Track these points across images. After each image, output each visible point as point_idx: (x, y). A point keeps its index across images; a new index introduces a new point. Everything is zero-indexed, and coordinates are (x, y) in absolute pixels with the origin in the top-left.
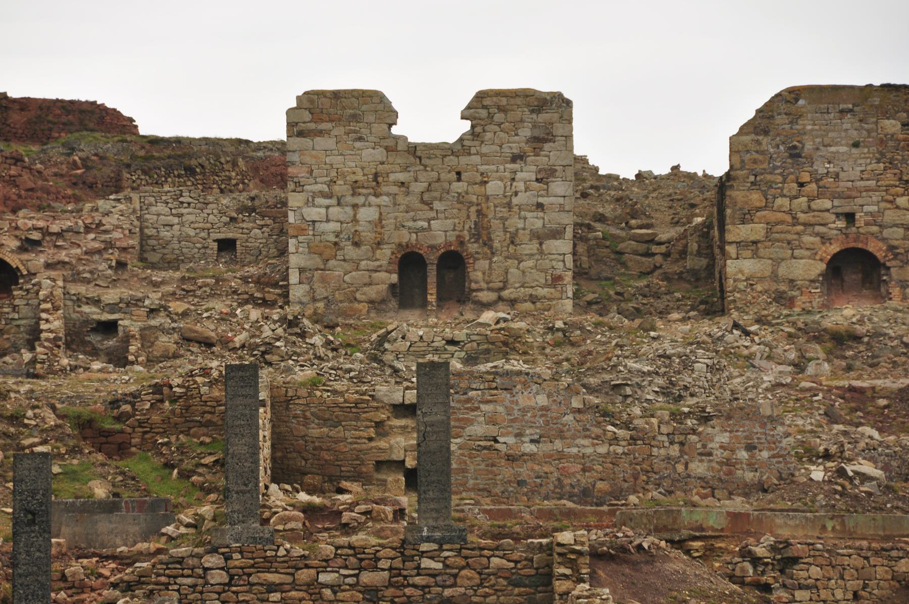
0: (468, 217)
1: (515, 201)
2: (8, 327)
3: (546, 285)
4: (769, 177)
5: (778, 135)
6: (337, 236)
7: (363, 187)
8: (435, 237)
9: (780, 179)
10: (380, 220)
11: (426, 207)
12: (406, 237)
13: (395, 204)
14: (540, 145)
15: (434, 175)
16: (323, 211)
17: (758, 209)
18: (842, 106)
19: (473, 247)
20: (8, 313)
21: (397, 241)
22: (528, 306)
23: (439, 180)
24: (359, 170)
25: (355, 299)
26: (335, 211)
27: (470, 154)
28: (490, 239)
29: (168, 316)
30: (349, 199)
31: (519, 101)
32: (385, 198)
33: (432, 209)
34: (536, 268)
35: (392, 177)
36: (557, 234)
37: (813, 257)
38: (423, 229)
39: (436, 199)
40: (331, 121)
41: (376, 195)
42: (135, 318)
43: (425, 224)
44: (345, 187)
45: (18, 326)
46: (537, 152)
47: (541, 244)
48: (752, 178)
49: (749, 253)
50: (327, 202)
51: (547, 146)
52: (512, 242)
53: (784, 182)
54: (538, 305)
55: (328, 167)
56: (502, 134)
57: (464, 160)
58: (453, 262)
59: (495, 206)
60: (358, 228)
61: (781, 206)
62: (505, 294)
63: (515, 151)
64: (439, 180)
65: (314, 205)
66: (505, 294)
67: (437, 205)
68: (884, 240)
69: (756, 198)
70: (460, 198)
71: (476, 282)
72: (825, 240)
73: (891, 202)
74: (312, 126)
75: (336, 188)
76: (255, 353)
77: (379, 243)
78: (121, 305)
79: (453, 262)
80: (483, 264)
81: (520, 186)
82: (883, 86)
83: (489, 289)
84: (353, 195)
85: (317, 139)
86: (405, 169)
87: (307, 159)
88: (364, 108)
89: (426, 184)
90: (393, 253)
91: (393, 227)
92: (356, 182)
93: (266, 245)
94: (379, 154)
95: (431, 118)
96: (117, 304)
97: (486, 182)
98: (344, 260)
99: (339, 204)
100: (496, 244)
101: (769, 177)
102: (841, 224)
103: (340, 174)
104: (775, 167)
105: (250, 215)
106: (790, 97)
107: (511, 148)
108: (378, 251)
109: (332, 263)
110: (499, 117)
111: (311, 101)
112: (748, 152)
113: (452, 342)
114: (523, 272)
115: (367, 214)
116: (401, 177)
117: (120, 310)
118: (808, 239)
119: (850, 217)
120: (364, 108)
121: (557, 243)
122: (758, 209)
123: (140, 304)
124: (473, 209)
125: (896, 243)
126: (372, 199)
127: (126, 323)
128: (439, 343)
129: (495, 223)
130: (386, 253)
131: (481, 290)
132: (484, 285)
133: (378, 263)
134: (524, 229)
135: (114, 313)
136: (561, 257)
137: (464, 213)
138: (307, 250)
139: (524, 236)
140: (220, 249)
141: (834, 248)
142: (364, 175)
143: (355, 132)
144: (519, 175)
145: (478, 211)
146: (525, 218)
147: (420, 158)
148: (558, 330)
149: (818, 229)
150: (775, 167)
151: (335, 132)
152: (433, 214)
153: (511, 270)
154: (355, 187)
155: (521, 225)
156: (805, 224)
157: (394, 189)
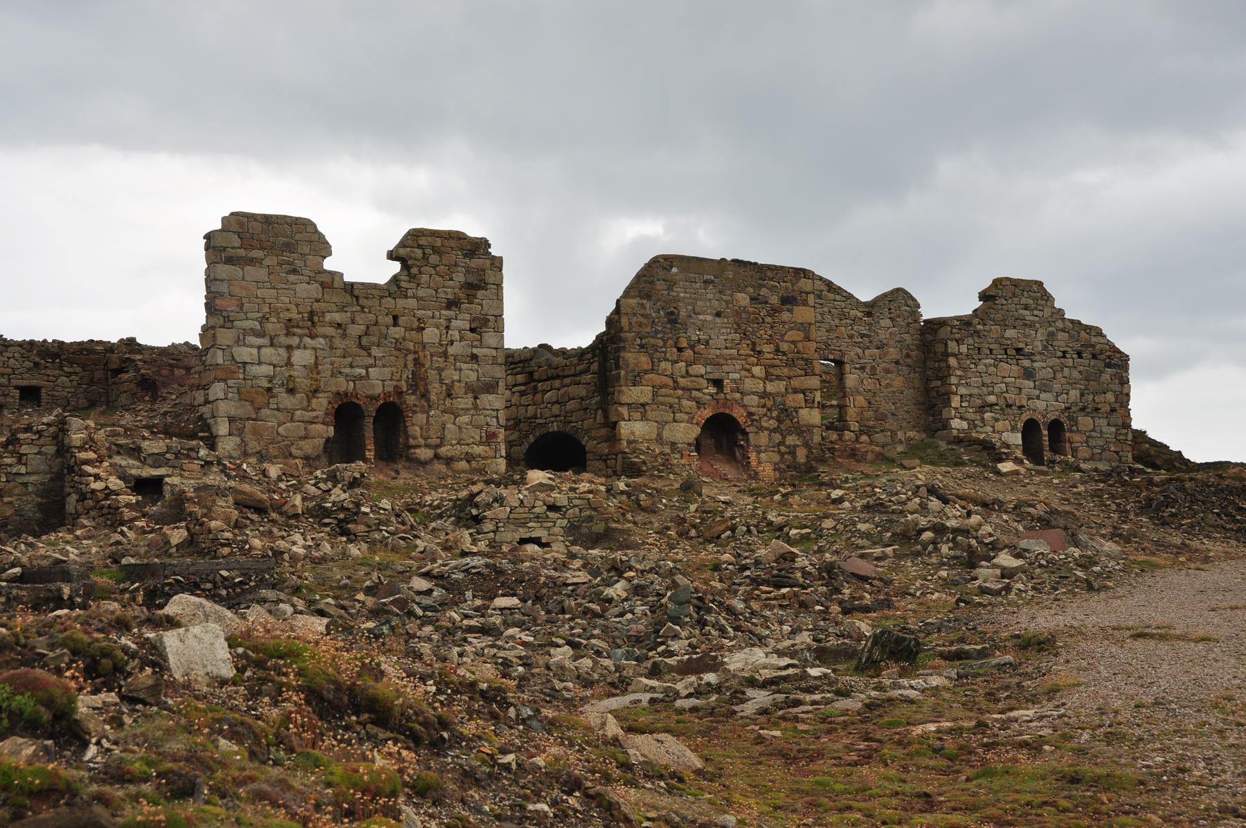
0: (406, 366)
1: (451, 350)
2: (11, 484)
3: (481, 443)
4: (652, 341)
5: (658, 300)
6: (270, 382)
7: (298, 327)
8: (373, 387)
9: (661, 343)
10: (316, 364)
11: (364, 353)
12: (343, 385)
13: (331, 348)
14: (473, 292)
16: (255, 351)
17: (646, 372)
18: (706, 277)
20: (11, 465)
21: (334, 389)
23: (376, 323)
24: (294, 307)
25: (291, 454)
26: (268, 352)
27: (406, 297)
28: (427, 391)
29: (222, 471)
30: (283, 340)
31: (453, 243)
32: (321, 340)
33: (370, 355)
34: (466, 426)
35: (328, 317)
36: (490, 388)
37: (690, 421)
38: (361, 378)
39: (374, 344)
40: (262, 248)
41: (312, 337)
42: (186, 474)
44: (278, 325)
45: (25, 484)
46: (471, 299)
47: (476, 398)
48: (638, 341)
49: (637, 415)
50: (260, 341)
51: (480, 294)
52: (449, 395)
53: (664, 346)
54: (474, 464)
55: (260, 301)
56: (438, 278)
57: (401, 303)
59: (432, 356)
60: (292, 373)
61: (665, 370)
62: (443, 451)
63: (450, 297)
64: (376, 323)
65: (245, 345)
66: (443, 451)
67: (375, 351)
68: (744, 406)
69: (644, 361)
70: (398, 345)
71: (415, 438)
72: (700, 404)
73: (748, 370)
74: (242, 252)
75: (269, 326)
76: (327, 521)
77: (316, 391)
78: (168, 456)
79: (391, 416)
80: (420, 418)
81: (456, 336)
82: (733, 261)
83: (427, 446)
84: (287, 335)
85: (247, 268)
86: (342, 309)
87: (237, 291)
88: (298, 237)
89: (364, 328)
90: (330, 403)
91: (329, 373)
92: (290, 320)
93: (74, 394)
94: (314, 290)
95: (361, 253)
96: (162, 454)
97: (423, 329)
98: (278, 409)
99: (272, 345)
100: (433, 397)
101: (652, 341)
102: (712, 390)
103: (274, 311)
104: (657, 332)
105: (53, 362)
106: (666, 264)
107: (446, 293)
108: (314, 401)
109: (265, 412)
110: (434, 259)
111: (241, 224)
112: (634, 314)
113: (553, 508)
114: (460, 428)
115: (302, 358)
116: (338, 317)
117: (167, 463)
118: (686, 403)
119: (718, 383)
120: (298, 237)
121: (491, 397)
122: (646, 372)
123: (193, 454)
124: (410, 357)
125: (753, 410)
126: (307, 340)
127: (176, 480)
128: (540, 509)
129: (433, 374)
130: (322, 403)
131: (418, 446)
132: (422, 442)
133: (314, 414)
134: (459, 381)
135: (160, 466)
136: (494, 414)
137: (402, 361)
138: (237, 396)
139: (459, 389)
140: (22, 398)
141: (707, 413)
142: (299, 313)
143: (288, 263)
144: (454, 323)
145: (415, 360)
146: (461, 370)
147: (357, 298)
148: (622, 492)
149: (695, 393)
150: (657, 332)
151: (267, 262)
152: (371, 361)
153: (448, 426)
154: (289, 325)
155: (456, 378)
156: (683, 389)
157: (330, 331)
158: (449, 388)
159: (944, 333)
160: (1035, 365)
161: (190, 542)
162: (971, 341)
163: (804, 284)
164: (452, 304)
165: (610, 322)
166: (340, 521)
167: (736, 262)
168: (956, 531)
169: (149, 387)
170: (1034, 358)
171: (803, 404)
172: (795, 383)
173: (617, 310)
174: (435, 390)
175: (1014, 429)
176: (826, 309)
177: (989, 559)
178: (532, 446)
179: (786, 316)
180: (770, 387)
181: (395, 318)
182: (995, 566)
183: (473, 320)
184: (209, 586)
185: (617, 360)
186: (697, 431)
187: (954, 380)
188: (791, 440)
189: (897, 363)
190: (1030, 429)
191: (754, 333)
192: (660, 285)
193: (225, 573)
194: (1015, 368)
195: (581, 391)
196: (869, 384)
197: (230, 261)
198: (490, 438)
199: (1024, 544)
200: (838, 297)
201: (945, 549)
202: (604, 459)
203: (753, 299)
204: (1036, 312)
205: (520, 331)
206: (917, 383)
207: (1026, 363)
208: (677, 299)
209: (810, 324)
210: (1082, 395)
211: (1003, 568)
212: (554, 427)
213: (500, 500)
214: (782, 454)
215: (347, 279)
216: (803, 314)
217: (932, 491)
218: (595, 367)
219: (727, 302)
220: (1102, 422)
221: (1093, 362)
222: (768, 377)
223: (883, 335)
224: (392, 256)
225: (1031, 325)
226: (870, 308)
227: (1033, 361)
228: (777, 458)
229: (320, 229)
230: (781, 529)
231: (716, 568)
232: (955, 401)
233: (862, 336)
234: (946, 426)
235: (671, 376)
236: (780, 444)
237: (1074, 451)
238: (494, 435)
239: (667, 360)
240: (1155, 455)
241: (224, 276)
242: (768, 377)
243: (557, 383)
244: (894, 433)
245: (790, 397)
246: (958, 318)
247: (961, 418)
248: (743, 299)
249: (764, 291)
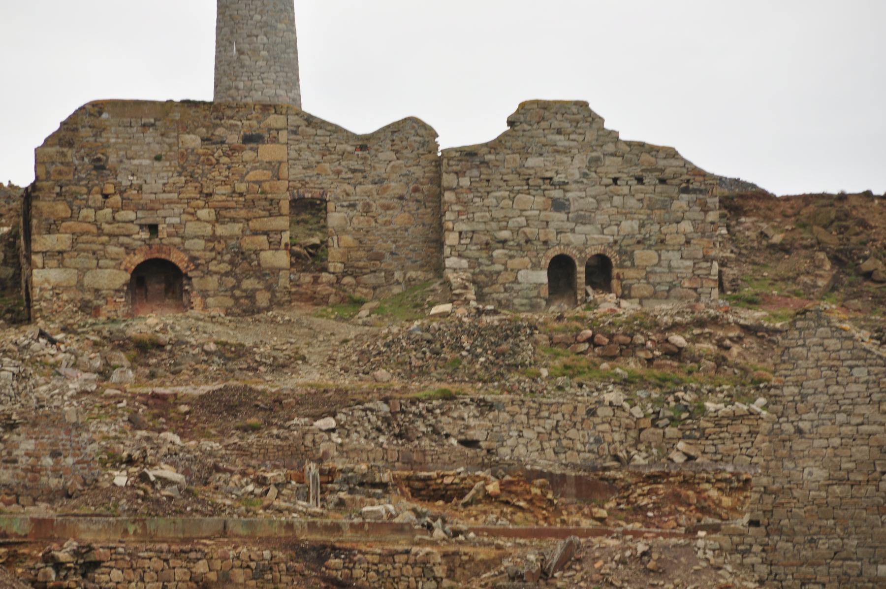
4: (74, 188)
5: (83, 147)
9: (85, 190)
17: (64, 220)
18: (144, 121)
37: (117, 267)
48: (57, 189)
61: (87, 217)
68: (185, 251)
69: (61, 209)
72: (129, 250)
73: (192, 214)
101: (74, 188)
102: (145, 235)
104: (80, 179)
112: (53, 163)
118: (113, 249)
119: (153, 229)
122: (64, 220)
125: (197, 254)
149: (123, 239)
150: (80, 179)
160: (569, 195)
162: (475, 172)
167: (187, 103)
170: (567, 187)
171: (266, 246)
172: (255, 224)
175: (535, 266)
176: (303, 145)
179: (248, 155)
180: (220, 230)
188: (248, 284)
189: (401, 198)
191: (203, 174)
194: (539, 200)
196: (360, 221)
200: (319, 132)
204: (572, 137)
206: (428, 220)
207: (557, 193)
209: (280, 163)
210: (642, 226)
214: (237, 299)
216: (268, 152)
219: (170, 145)
220: (673, 257)
221: (660, 188)
222: (219, 219)
223: (381, 170)
225: (566, 151)
227: (565, 191)
228: (230, 302)
233: (354, 171)
235: (95, 222)
236: (234, 288)
239: (90, 207)
242: (219, 219)
244: (390, 274)
245: (248, 240)
247: (460, 256)
248: (192, 140)
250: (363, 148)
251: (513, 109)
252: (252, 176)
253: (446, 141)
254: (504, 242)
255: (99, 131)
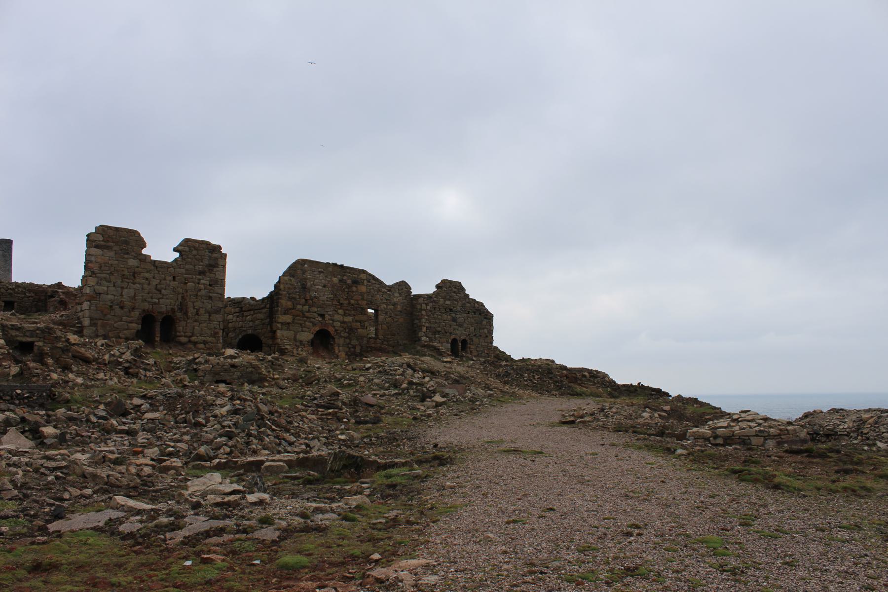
3: (211, 336)
12: (146, 306)
15: (163, 276)
16: (105, 288)
19: (179, 315)
22: (202, 346)
38: (155, 303)
41: (134, 283)
43: (157, 301)
46: (211, 271)
51: (215, 269)
52: (197, 314)
58: (169, 322)
68: (334, 327)
69: (289, 304)
70: (174, 290)
79: (169, 322)
83: (185, 336)
95: (161, 249)
100: (190, 314)
111: (103, 230)
115: (128, 293)
121: (217, 316)
129: (190, 304)
130: (136, 313)
139: (202, 311)
141: (317, 329)
144: (202, 282)
158: (198, 310)
159: (420, 301)
161: (20, 374)
163: (363, 276)
164: (202, 273)
165: (276, 286)
166: (126, 368)
168: (416, 384)
169: (63, 304)
173: (279, 282)
174: (191, 311)
175: (447, 342)
177: (431, 397)
178: (240, 340)
181: (174, 278)
182: (433, 401)
183: (211, 281)
184: (8, 398)
185: (278, 303)
186: (312, 336)
187: (424, 320)
190: (454, 342)
192: (299, 272)
193: (19, 391)
195: (261, 316)
197: (97, 247)
198: (215, 335)
199: (447, 391)
201: (411, 392)
202: (269, 346)
203: (340, 281)
205: (234, 289)
207: (454, 315)
208: (306, 279)
211: (437, 402)
212: (250, 332)
213: (207, 361)
215: (152, 258)
217: (409, 366)
218: (268, 306)
222: (345, 315)
224: (175, 250)
226: (391, 288)
228: (347, 350)
229: (142, 235)
230: (340, 380)
231: (302, 398)
232: (424, 329)
234: (420, 339)
237: (471, 352)
238: (217, 333)
240: (501, 356)
241: (93, 253)
242: (345, 315)
243: (252, 312)
246: (427, 295)
248: (335, 280)
249: (345, 278)
250: (389, 291)
251: (439, 281)
252: (356, 297)
253: (415, 291)
254: (439, 332)
255: (304, 272)
